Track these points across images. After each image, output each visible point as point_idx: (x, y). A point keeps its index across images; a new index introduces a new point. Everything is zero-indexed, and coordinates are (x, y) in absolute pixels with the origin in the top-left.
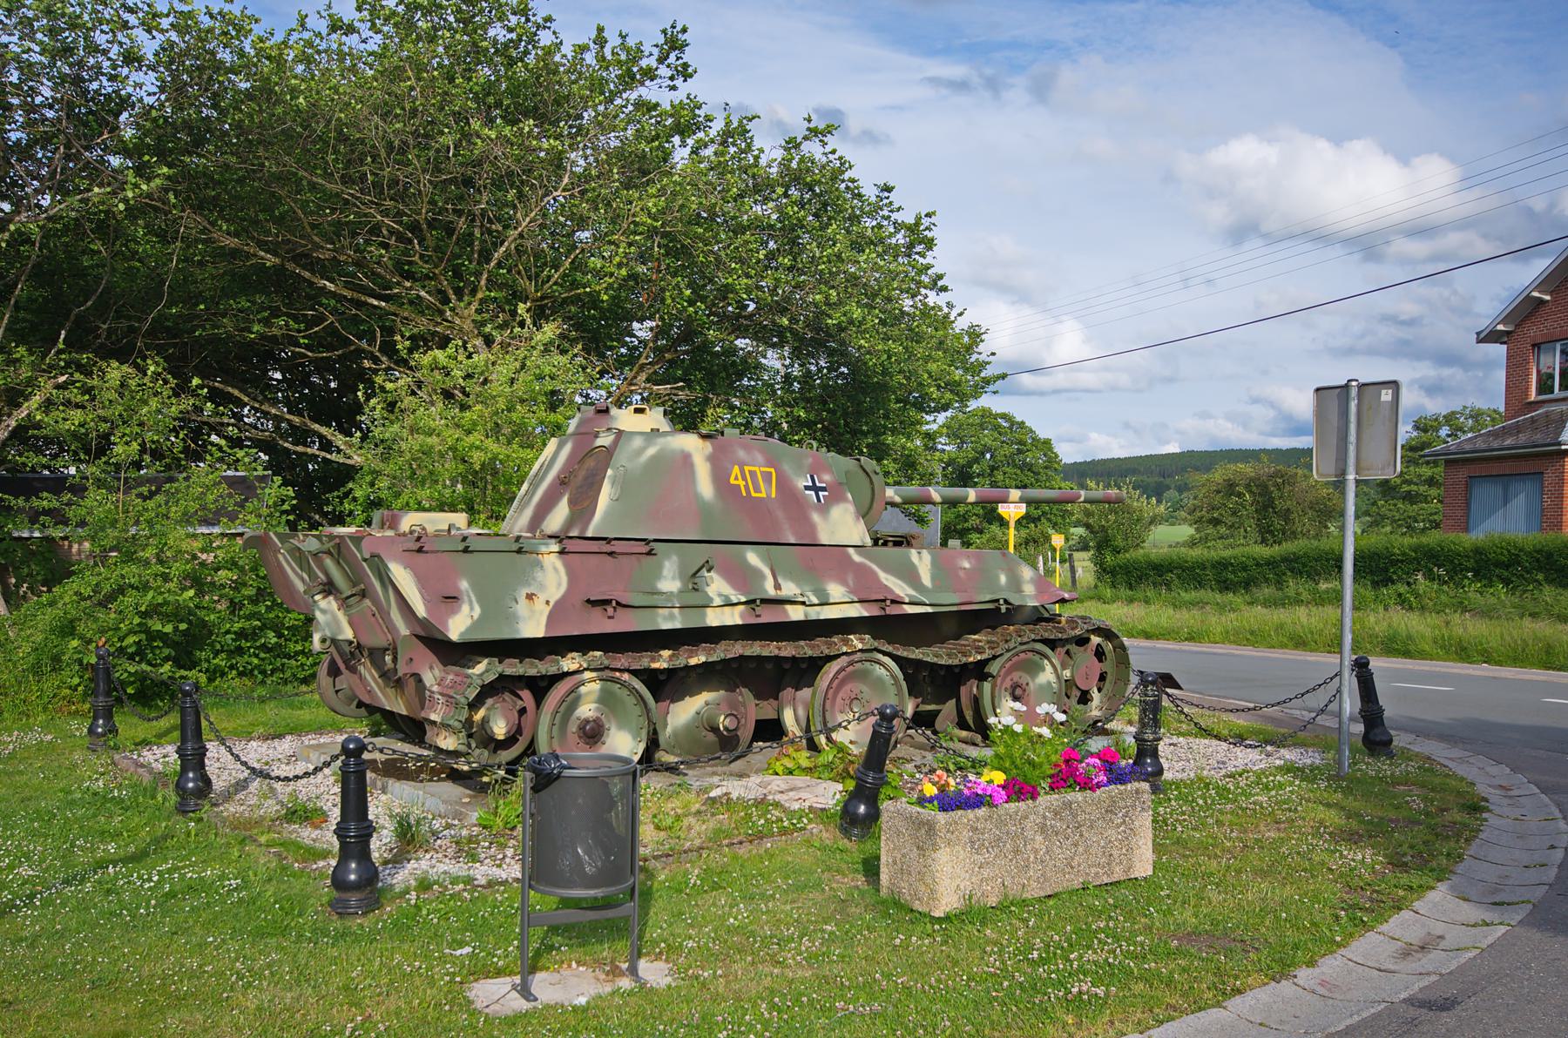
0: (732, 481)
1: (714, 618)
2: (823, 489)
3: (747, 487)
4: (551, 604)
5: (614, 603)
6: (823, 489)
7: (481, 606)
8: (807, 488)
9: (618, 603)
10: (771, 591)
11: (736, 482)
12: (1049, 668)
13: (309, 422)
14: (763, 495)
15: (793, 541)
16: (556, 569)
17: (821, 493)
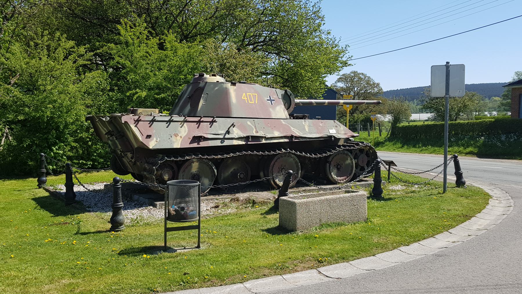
0: (243, 98)
2: (274, 100)
3: (247, 100)
6: (274, 100)
8: (268, 100)
11: (244, 98)
12: (349, 159)
13: (298, 179)
14: (253, 102)
15: (282, 120)
17: (273, 102)
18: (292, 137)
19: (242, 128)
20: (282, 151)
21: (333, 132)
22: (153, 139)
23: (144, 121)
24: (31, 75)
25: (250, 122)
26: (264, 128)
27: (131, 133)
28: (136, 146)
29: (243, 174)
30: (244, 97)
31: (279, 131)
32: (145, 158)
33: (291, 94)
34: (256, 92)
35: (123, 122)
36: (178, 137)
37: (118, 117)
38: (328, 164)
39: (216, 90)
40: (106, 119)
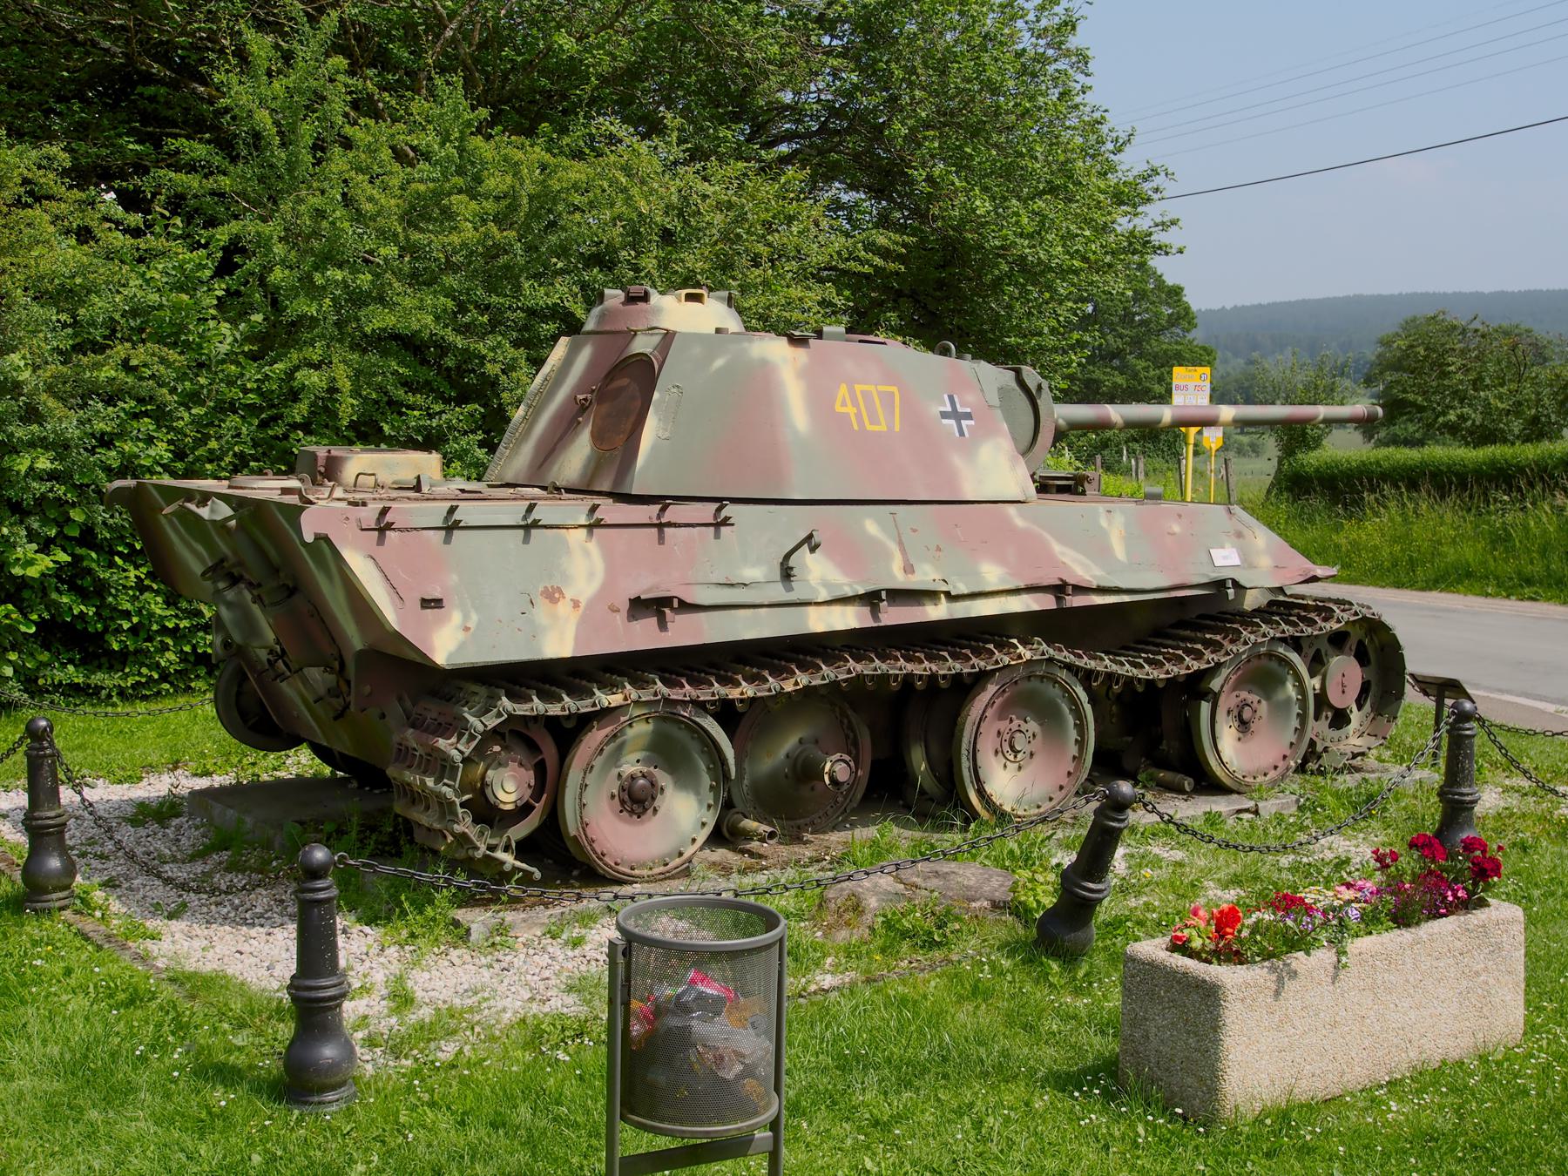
1: (821, 621)
2: (968, 416)
3: (859, 416)
4: (583, 605)
6: (968, 416)
8: (944, 415)
9: (681, 602)
11: (843, 410)
14: (883, 428)
15: (1011, 509)
18: (1059, 589)
19: (851, 554)
20: (1020, 657)
21: (1226, 560)
23: (407, 530)
26: (939, 549)
27: (337, 579)
28: (356, 640)
29: (844, 765)
31: (1001, 560)
32: (400, 699)
33: (1039, 388)
34: (890, 378)
35: (309, 538)
37: (273, 507)
38: (1205, 707)
40: (212, 511)
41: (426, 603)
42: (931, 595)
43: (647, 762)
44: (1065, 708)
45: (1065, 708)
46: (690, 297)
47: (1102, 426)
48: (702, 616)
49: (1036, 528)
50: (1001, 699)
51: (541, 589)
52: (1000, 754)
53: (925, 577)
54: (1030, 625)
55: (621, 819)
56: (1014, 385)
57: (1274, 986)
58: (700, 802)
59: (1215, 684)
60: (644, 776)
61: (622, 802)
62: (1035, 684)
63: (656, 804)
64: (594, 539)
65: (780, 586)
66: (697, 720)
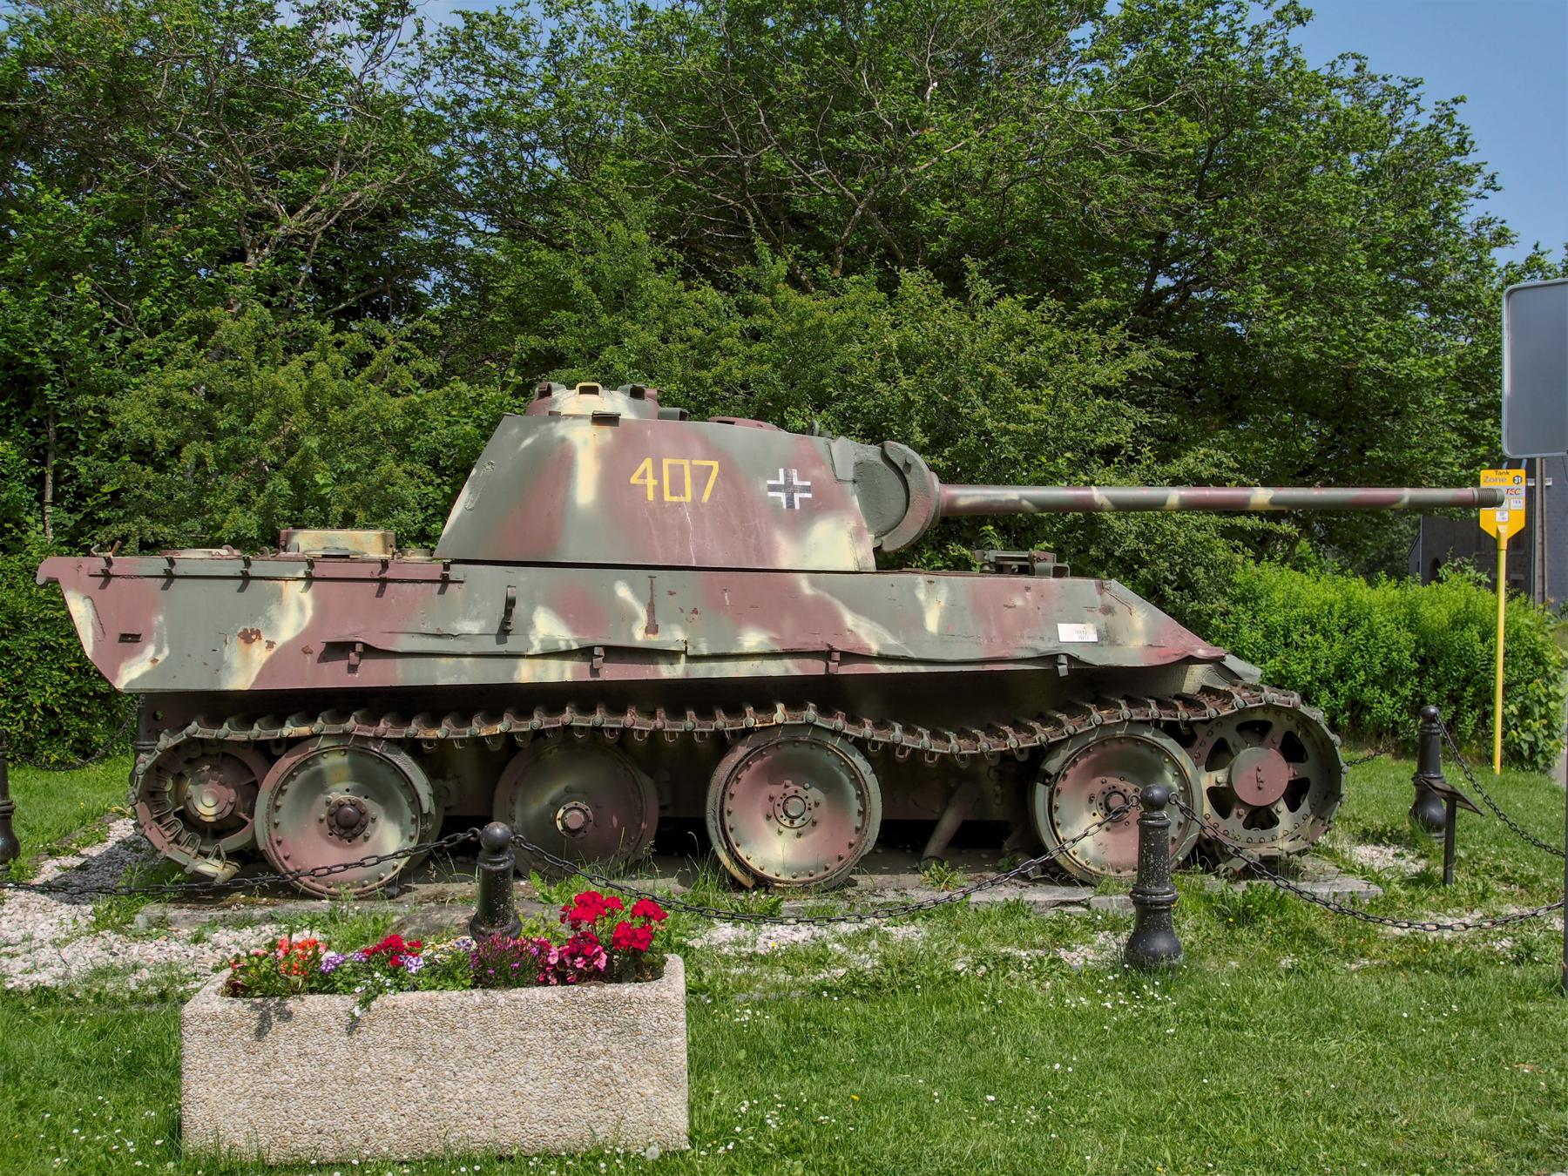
1: (526, 673)
4: (276, 647)
5: (359, 648)
7: (171, 649)
9: (367, 647)
10: (639, 637)
16: (301, 608)
22: (141, 651)
24: (120, 62)
25: (633, 587)
26: (695, 611)
30: (644, 476)
31: (762, 623)
34: (712, 453)
36: (256, 644)
38: (1041, 792)
39: (529, 448)
41: (125, 638)
42: (671, 656)
43: (356, 791)
44: (845, 778)
45: (845, 778)
46: (584, 390)
47: (1157, 505)
48: (399, 662)
49: (827, 596)
50: (758, 763)
51: (240, 630)
52: (773, 819)
53: (673, 636)
54: (793, 692)
55: (330, 841)
56: (878, 459)
57: (255, 1024)
58: (403, 833)
59: (1052, 765)
60: (352, 805)
61: (331, 827)
62: (801, 750)
63: (368, 831)
64: (310, 591)
65: (493, 639)
66: (389, 755)
